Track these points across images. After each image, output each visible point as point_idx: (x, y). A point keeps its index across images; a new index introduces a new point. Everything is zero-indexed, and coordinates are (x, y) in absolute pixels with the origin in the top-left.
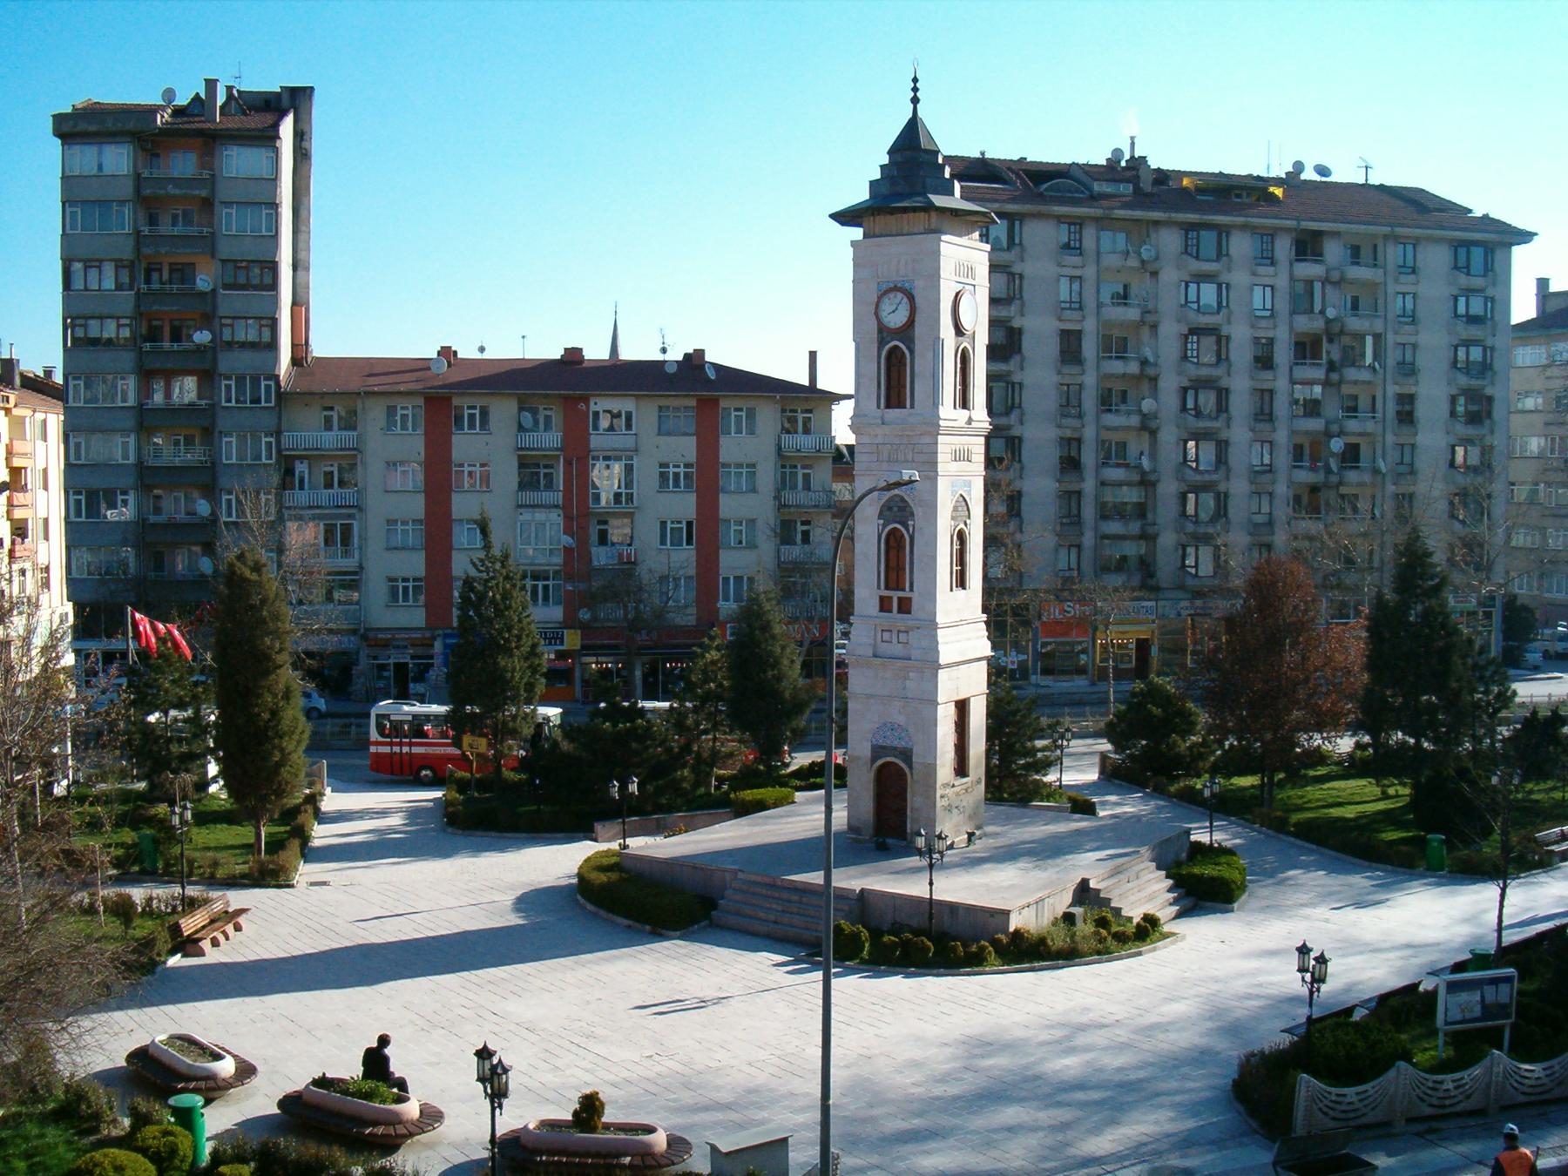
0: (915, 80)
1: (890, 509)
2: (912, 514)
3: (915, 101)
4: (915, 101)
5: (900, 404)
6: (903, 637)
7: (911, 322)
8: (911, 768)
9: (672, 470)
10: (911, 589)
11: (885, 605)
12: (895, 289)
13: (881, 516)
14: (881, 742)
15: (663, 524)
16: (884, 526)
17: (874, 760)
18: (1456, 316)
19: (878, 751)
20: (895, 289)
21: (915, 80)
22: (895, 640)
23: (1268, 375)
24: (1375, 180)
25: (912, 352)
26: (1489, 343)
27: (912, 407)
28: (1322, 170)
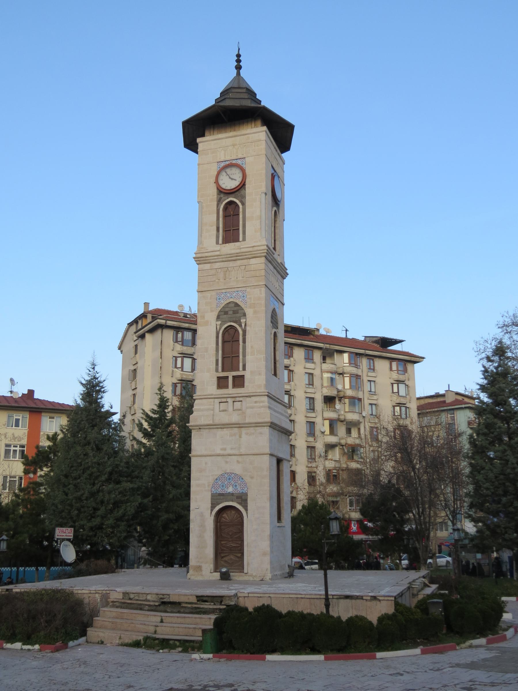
0: (238, 56)
1: (226, 313)
2: (245, 315)
3: (238, 68)
4: (238, 68)
5: (236, 240)
6: (237, 405)
7: (242, 186)
8: (246, 510)
9: (12, 448)
10: (244, 369)
11: (222, 383)
12: (231, 165)
13: (218, 318)
14: (220, 491)
15: (5, 478)
16: (221, 325)
17: (213, 507)
18: (393, 392)
19: (216, 498)
20: (231, 165)
21: (238, 56)
22: (231, 409)
23: (313, 415)
24: (350, 336)
25: (243, 204)
26: (407, 405)
27: (244, 239)
28: (328, 331)
